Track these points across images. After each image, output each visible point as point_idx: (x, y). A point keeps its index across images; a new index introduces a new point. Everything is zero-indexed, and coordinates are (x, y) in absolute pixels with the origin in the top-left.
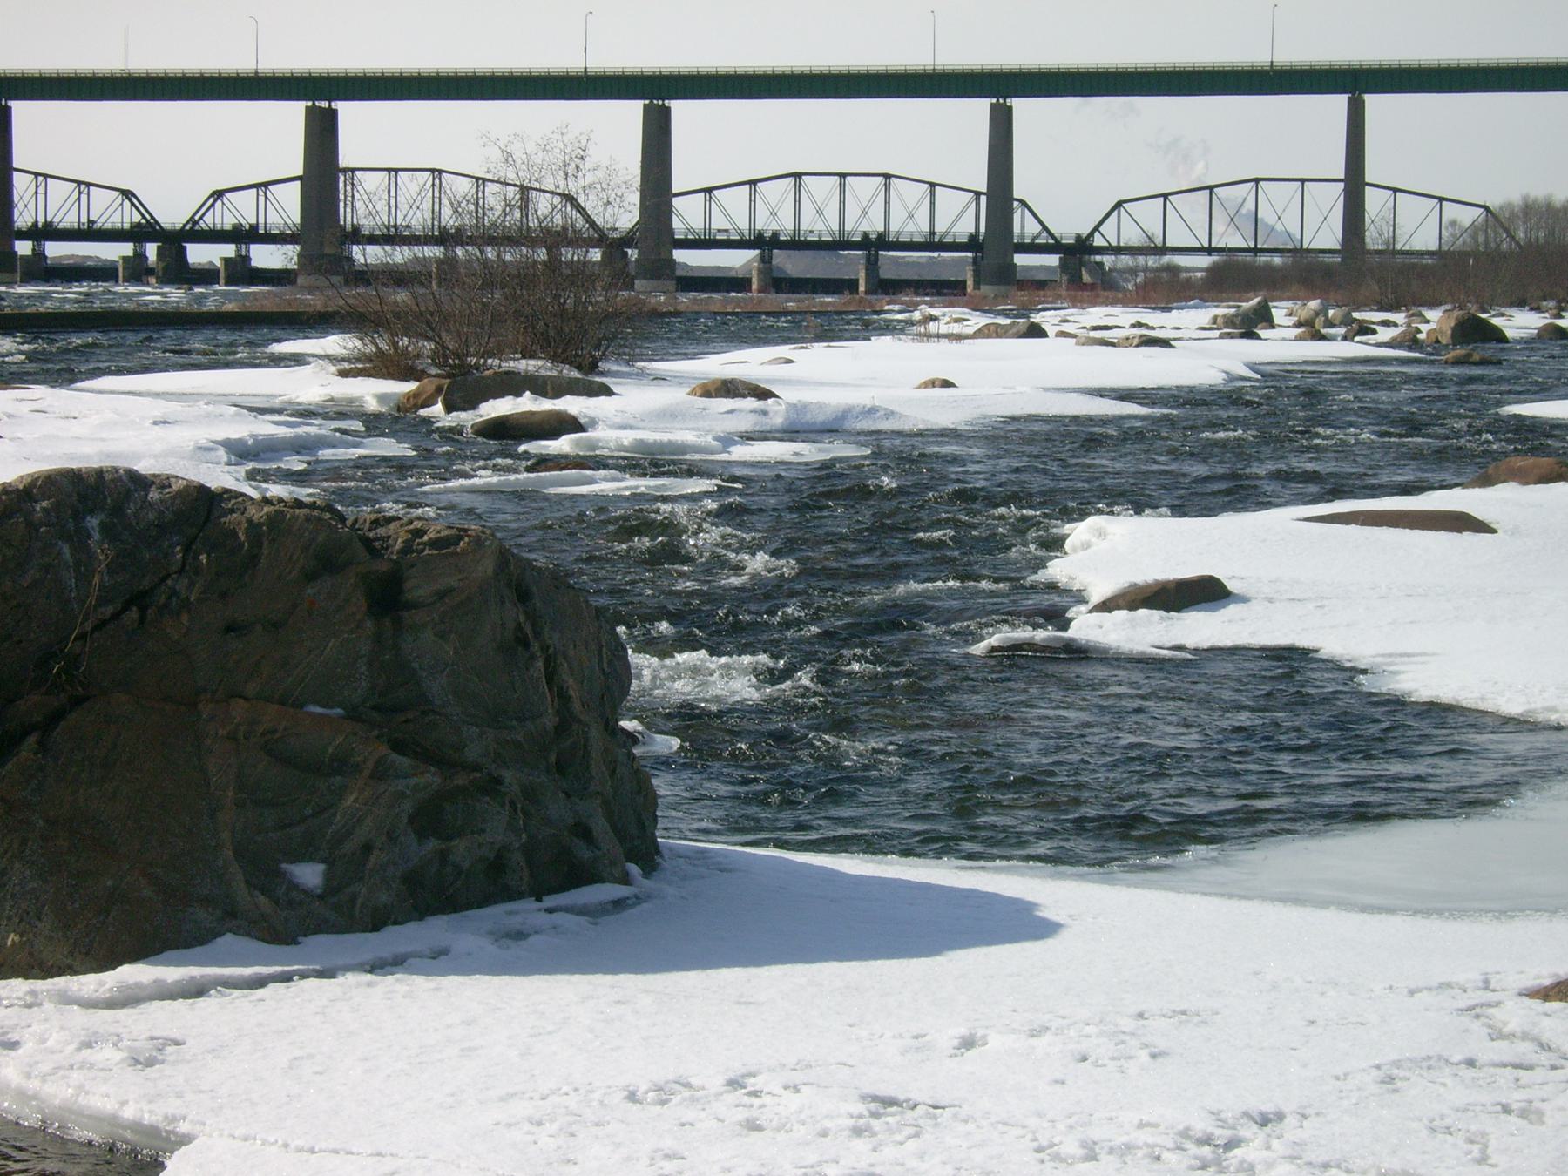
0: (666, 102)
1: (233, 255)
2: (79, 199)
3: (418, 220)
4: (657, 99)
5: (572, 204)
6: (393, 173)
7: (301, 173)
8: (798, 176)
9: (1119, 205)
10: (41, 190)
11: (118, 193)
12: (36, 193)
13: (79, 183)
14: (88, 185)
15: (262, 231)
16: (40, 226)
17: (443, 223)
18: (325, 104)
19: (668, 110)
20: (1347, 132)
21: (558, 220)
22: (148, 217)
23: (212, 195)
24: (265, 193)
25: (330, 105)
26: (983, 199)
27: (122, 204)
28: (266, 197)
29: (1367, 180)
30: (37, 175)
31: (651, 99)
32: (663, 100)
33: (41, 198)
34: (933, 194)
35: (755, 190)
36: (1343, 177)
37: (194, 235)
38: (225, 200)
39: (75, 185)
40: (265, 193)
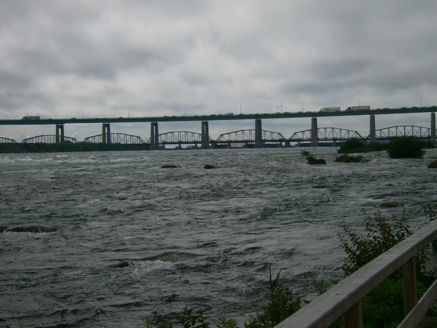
1: (297, 144)
3: (331, 137)
7: (311, 129)
8: (397, 126)
18: (315, 117)
20: (151, 129)
21: (354, 136)
23: (221, 135)
26: (430, 130)
29: (262, 130)
31: (313, 117)
32: (434, 112)
34: (421, 129)
37: (291, 140)
38: (223, 136)
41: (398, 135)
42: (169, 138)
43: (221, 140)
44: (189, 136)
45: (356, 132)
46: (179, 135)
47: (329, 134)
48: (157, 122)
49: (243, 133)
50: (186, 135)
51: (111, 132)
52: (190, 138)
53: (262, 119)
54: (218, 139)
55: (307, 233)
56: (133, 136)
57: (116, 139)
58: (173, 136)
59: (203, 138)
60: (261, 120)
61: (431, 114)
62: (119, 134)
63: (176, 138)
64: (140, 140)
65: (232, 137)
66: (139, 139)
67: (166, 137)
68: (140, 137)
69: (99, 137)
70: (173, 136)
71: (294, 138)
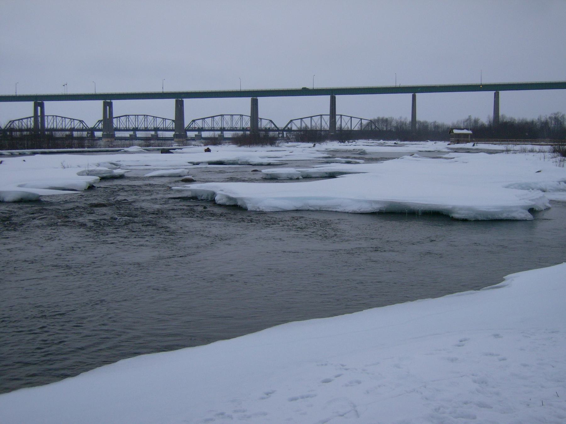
0: (183, 99)
2: (163, 122)
5: (271, 122)
8: (321, 115)
9: (291, 121)
10: (155, 120)
11: (79, 121)
12: (154, 121)
13: (163, 119)
14: (165, 119)
16: (222, 128)
17: (243, 127)
19: (257, 100)
21: (268, 126)
22: (86, 126)
27: (80, 125)
30: (154, 117)
31: (105, 100)
33: (155, 122)
36: (329, 114)
39: (162, 119)
41: (58, 128)
42: (123, 124)
43: (99, 128)
45: (271, 121)
46: (137, 120)
47: (237, 123)
48: (183, 99)
49: (222, 118)
51: (46, 113)
52: (151, 124)
53: (336, 96)
54: (189, 126)
55: (550, 191)
56: (74, 119)
57: (51, 124)
58: (127, 120)
59: (36, 121)
62: (55, 117)
63: (132, 123)
64: (83, 125)
66: (82, 124)
67: (118, 122)
68: (83, 121)
69: (28, 121)
70: (127, 120)
71: (192, 126)
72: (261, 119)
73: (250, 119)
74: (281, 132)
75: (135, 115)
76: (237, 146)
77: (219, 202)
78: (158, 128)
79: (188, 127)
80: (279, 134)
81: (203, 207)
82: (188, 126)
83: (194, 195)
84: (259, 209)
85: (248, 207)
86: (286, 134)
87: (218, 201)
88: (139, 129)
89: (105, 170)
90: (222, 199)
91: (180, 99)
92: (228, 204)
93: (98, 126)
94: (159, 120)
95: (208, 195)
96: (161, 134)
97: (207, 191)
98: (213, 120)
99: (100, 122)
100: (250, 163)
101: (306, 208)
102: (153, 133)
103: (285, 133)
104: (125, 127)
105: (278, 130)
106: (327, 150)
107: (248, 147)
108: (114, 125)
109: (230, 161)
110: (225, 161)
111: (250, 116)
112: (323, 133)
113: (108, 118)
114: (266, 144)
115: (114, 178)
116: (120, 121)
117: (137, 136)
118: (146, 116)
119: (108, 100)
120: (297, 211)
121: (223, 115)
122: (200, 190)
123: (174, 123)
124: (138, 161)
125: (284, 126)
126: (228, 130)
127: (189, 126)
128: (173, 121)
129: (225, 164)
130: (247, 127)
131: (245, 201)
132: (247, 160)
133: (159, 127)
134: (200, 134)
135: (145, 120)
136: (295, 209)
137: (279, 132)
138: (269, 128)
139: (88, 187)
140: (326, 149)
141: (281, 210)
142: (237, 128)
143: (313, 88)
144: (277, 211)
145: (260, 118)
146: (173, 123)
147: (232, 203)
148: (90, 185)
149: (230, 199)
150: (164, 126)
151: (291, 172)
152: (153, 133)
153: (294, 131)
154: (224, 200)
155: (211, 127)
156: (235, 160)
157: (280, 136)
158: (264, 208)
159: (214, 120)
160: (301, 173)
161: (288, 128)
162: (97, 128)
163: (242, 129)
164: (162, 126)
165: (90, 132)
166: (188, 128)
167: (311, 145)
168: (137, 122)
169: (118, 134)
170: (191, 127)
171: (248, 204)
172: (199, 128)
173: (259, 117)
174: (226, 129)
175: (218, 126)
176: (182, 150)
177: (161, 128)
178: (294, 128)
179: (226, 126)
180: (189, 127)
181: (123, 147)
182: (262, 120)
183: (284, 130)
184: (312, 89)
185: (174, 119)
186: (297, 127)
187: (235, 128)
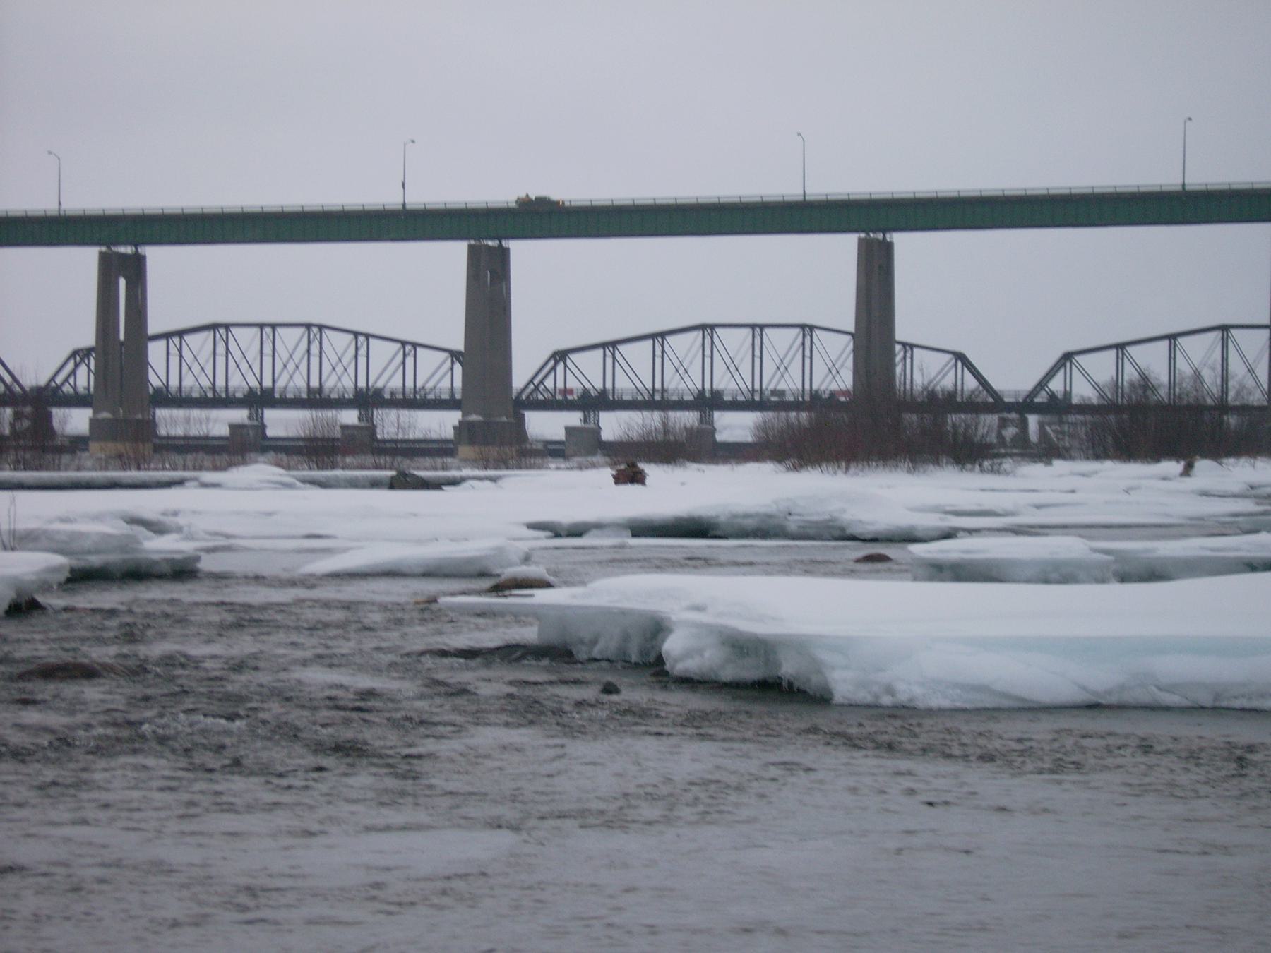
0: (504, 243)
2: (404, 363)
4: (874, 232)
6: (222, 331)
8: (1224, 328)
9: (1068, 357)
10: (362, 351)
12: (308, 351)
13: (404, 344)
15: (959, 399)
16: (708, 395)
17: (815, 387)
21: (948, 383)
24: (613, 354)
25: (884, 237)
28: (614, 358)
30: (356, 334)
31: (867, 232)
32: (884, 231)
33: (362, 361)
35: (1175, 345)
40: (613, 354)
42: (196, 369)
43: (75, 388)
44: (285, 356)
45: (960, 357)
46: (268, 349)
47: (783, 369)
48: (504, 243)
49: (708, 340)
50: (315, 349)
54: (536, 382)
58: (221, 349)
60: (504, 254)
61: (856, 241)
65: (1076, 363)
67: (174, 361)
70: (221, 349)
71: (549, 383)
72: (908, 346)
73: (851, 346)
74: (1014, 416)
75: (261, 326)
76: (780, 467)
77: (680, 667)
78: (378, 393)
79: (532, 386)
80: (1003, 423)
81: (600, 687)
82: (531, 381)
83: (553, 637)
84: (893, 695)
85: (833, 685)
86: (1041, 425)
87: (676, 661)
88: (277, 396)
89: (97, 534)
90: (700, 651)
91: (490, 243)
92: (728, 674)
93: (71, 381)
94: (382, 353)
95: (626, 638)
96: (390, 423)
97: (624, 613)
98: (658, 352)
99: (82, 360)
100: (850, 531)
101: (1143, 697)
102: (350, 417)
103: (1033, 420)
104: (206, 383)
105: (996, 404)
106: (1253, 492)
107: (840, 473)
108: (150, 372)
109: (746, 516)
110: (717, 517)
111: (852, 328)
112: (1232, 420)
113: (122, 337)
114: (937, 462)
115: (138, 573)
116: (181, 356)
117: (270, 432)
118: (315, 330)
119: (125, 243)
120: (1093, 707)
121: (712, 327)
122: (586, 607)
123: (458, 368)
124: (270, 514)
125: (1026, 384)
126: (735, 406)
127: (535, 383)
128: (454, 355)
129: (718, 533)
130: (834, 387)
131: (824, 656)
132: (836, 515)
133: (380, 384)
134: (592, 425)
135: (308, 351)
136: (1081, 697)
137: (1005, 415)
138: (951, 396)
139: (10, 607)
140: (1252, 487)
141: (1006, 703)
142: (782, 393)
143: (1184, 185)
144: (988, 705)
145: (904, 345)
146: (452, 369)
147: (749, 671)
148: (19, 594)
149: (741, 645)
150: (410, 384)
151: (1063, 555)
152: (350, 417)
153: (1084, 408)
154: (707, 654)
155: (649, 386)
156: (770, 516)
157: (1008, 439)
158: (918, 691)
159: (663, 351)
160: (1116, 561)
161: (1052, 396)
162: (67, 389)
163: (807, 398)
164: (396, 383)
165: (28, 409)
166: (528, 391)
167: (1172, 467)
168: (267, 361)
169: (171, 422)
170: (547, 389)
171: (833, 668)
172: (586, 391)
173: (899, 336)
174: (727, 398)
175: (683, 383)
176: (500, 483)
177: (392, 393)
178: (1082, 391)
179: (724, 383)
180: (536, 388)
181: (195, 469)
182: (916, 350)
183: (1026, 405)
184: (1177, 192)
185: (459, 345)
186: (1096, 386)
187: (774, 392)
